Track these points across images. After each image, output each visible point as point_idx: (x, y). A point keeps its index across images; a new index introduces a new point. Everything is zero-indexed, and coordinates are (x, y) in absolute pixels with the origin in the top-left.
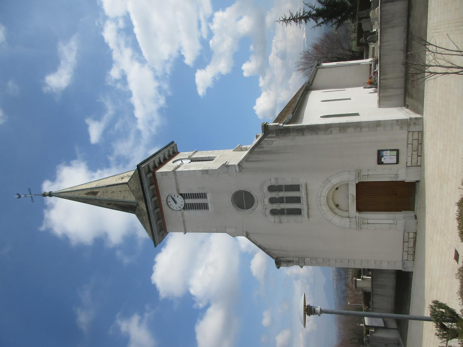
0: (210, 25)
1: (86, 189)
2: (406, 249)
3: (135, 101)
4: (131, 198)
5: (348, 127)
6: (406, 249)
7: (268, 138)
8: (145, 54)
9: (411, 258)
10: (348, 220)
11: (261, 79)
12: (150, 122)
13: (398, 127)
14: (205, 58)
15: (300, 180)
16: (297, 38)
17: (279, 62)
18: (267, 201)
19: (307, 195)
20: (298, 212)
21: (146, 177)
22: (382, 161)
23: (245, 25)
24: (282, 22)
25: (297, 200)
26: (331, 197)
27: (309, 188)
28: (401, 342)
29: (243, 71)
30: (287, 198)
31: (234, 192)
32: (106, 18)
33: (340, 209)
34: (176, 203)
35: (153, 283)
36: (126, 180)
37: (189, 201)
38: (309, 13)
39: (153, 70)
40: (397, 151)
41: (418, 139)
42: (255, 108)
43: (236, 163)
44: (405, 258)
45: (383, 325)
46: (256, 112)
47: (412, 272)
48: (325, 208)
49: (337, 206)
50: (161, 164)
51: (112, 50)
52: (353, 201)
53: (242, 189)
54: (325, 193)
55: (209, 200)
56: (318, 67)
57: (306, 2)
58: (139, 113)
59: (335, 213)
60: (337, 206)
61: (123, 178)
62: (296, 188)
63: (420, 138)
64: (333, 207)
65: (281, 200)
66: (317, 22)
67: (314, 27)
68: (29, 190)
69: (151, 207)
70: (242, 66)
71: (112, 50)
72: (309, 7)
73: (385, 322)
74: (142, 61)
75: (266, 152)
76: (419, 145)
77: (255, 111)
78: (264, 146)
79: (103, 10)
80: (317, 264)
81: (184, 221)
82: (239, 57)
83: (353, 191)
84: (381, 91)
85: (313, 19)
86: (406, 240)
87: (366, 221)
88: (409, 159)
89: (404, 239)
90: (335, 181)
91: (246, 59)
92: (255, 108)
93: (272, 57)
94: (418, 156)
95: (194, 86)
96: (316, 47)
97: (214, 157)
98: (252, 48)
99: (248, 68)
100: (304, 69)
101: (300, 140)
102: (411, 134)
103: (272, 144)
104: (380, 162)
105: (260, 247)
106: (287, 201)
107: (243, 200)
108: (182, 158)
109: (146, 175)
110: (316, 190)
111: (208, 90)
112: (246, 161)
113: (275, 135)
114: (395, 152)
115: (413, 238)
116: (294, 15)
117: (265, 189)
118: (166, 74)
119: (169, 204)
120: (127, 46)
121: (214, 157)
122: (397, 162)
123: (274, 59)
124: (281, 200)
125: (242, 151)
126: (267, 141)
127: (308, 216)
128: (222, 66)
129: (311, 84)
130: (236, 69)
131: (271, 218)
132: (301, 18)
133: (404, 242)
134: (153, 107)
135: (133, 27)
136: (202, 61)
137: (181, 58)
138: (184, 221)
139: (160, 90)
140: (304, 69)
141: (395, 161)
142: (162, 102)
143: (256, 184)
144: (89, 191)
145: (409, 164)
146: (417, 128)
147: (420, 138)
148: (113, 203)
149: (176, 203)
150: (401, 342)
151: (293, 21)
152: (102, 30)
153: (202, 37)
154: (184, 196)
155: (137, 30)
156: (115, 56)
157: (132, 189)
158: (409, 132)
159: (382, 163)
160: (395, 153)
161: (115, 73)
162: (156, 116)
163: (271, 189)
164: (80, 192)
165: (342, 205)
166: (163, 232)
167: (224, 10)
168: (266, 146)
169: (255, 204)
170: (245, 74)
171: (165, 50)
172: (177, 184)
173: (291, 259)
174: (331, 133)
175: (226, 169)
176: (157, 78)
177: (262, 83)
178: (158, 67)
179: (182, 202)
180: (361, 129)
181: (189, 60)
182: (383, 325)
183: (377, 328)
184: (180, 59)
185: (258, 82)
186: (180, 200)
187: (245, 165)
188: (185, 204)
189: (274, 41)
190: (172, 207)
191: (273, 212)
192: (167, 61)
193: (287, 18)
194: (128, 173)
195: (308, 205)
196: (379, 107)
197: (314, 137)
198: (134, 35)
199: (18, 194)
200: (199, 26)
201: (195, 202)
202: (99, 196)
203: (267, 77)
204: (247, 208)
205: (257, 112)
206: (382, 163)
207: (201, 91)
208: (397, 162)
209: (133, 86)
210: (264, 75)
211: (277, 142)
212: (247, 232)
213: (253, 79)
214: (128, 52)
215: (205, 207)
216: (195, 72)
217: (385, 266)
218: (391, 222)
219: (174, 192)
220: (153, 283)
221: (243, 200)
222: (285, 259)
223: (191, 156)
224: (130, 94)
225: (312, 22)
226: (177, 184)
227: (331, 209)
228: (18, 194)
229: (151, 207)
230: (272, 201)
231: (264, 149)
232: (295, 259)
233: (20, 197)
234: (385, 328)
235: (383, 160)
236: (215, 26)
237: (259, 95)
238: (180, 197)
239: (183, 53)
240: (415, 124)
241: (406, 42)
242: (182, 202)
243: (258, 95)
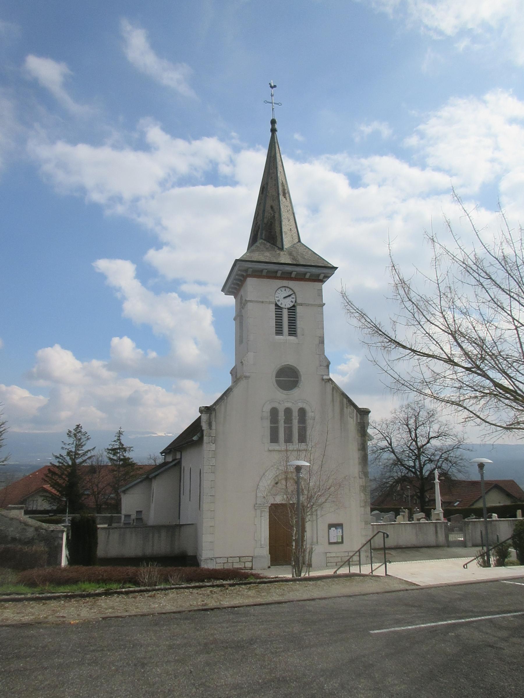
0: (198, 299)
2: (230, 560)
3: (105, 153)
6: (230, 560)
7: (357, 414)
8: (177, 191)
20: (274, 439)
22: (332, 529)
23: (188, 351)
29: (121, 337)
31: (279, 367)
32: (237, 150)
37: (285, 313)
40: (342, 542)
42: (57, 347)
43: (331, 376)
44: (219, 561)
46: (50, 349)
58: (83, 152)
62: (302, 439)
70: (129, 337)
71: (190, 143)
74: (163, 184)
75: (342, 410)
77: (52, 346)
78: (349, 409)
79: (248, 148)
81: (263, 302)
82: (145, 334)
86: (243, 560)
88: (333, 555)
89: (243, 557)
91: (139, 344)
92: (57, 347)
94: (336, 563)
98: (153, 354)
103: (350, 417)
104: (330, 526)
111: (103, 277)
112: (333, 388)
114: (340, 541)
115: (245, 567)
117: (300, 405)
118: (139, 215)
122: (330, 543)
126: (354, 412)
128: (136, 303)
131: (267, 408)
133: (240, 557)
135: (216, 185)
136: (146, 274)
137: (158, 245)
138: (263, 302)
139: (118, 199)
142: (96, 197)
143: (307, 395)
145: (328, 555)
148: (277, 215)
152: (222, 140)
153: (185, 282)
155: (210, 189)
156: (181, 144)
161: (155, 134)
163: (302, 412)
167: (213, 323)
169: (285, 392)
170: (116, 340)
172: (308, 305)
173: (214, 427)
174: (360, 478)
175: (325, 364)
176: (136, 199)
177: (96, 363)
179: (285, 305)
180: (363, 507)
181: (155, 257)
186: (287, 303)
187: (329, 386)
189: (159, 388)
191: (274, 412)
192: (158, 223)
197: (357, 461)
198: (204, 184)
200: (200, 283)
203: (105, 373)
204: (277, 381)
205: (49, 351)
207: (103, 264)
208: (330, 543)
209: (130, 158)
210: (110, 367)
211: (352, 423)
212: (249, 377)
213: (103, 351)
214: (183, 167)
216: (133, 262)
222: (214, 420)
226: (308, 305)
228: (275, 86)
231: (345, 409)
236: (193, 306)
242: (285, 305)
243: (79, 355)
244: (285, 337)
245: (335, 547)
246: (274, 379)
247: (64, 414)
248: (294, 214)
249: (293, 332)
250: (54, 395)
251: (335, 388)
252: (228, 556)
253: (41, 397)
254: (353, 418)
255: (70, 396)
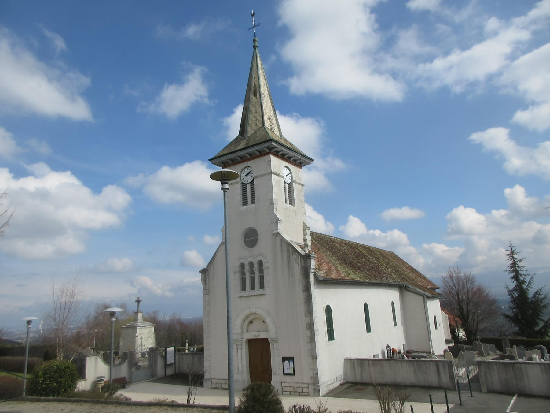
1: (259, 85)
2: (220, 381)
3: (455, 57)
4: (250, 131)
5: (311, 331)
6: (220, 381)
9: (214, 386)
10: (239, 331)
11: (503, 212)
12: (429, 79)
13: (312, 375)
14: (526, 138)
15: (268, 290)
16: (489, 269)
17: (530, 235)
18: (251, 259)
19: (257, 295)
21: (265, 147)
24: (510, 249)
25: (253, 287)
26: (257, 316)
27: (262, 297)
28: (155, 378)
30: (254, 277)
31: (257, 229)
33: (248, 325)
34: (247, 175)
35: (234, 110)
36: (267, 124)
37: (249, 187)
38: (524, 282)
39: (500, 74)
40: (294, 374)
41: (303, 392)
43: (279, 231)
44: (214, 381)
45: (167, 363)
47: (203, 387)
48: (247, 312)
49: (251, 322)
50: (283, 157)
51: (524, 14)
52: (255, 336)
53: (259, 237)
54: (259, 311)
55: (250, 206)
56: (425, 297)
57: (535, 277)
59: (244, 321)
60: (251, 322)
61: (270, 119)
62: (262, 286)
63: (304, 394)
64: (250, 319)
65: (252, 272)
66: (513, 290)
67: (507, 287)
68: (259, 25)
69: (240, 153)
70: (521, 185)
72: (530, 281)
73: (171, 365)
74: (512, 57)
75: (289, 257)
76: (298, 394)
80: (205, 306)
83: (262, 336)
84: (359, 361)
85: (516, 286)
87: (239, 347)
88: (287, 385)
90: (268, 320)
91: (529, 193)
92: (461, 208)
93: (536, 226)
95: (483, 127)
96: (480, 290)
97: (294, 205)
99: (518, 194)
100: (451, 277)
101: (299, 288)
102: (306, 386)
104: (284, 359)
105: (215, 255)
106: (252, 277)
107: (251, 238)
108: (293, 174)
109: (258, 151)
110: (262, 304)
111: (480, 146)
113: (303, 265)
116: (520, 264)
119: (246, 169)
120: (535, 33)
121: (294, 205)
123: (533, 228)
124: (252, 272)
125: (304, 230)
127: (241, 297)
128: (516, 162)
129: (406, 290)
130: (512, 180)
131: (237, 264)
132: (517, 272)
134: (449, 79)
139: (473, 84)
140: (451, 277)
141: (286, 372)
142: (458, 89)
143: (264, 249)
144: (258, 88)
146: (311, 392)
147: (304, 394)
149: (247, 175)
150: (155, 378)
151: (511, 262)
154: (252, 182)
156: (519, 20)
157: (258, 132)
158: (308, 384)
159: (283, 361)
160: (292, 372)
161: (492, 23)
162: (437, 85)
163: (261, 263)
164: (256, 78)
165: (252, 326)
166: (223, 165)
168: (294, 257)
169: (248, 249)
171: (533, 85)
172: (261, 176)
173: (207, 282)
176: (490, 77)
177: (499, 214)
178: (505, 79)
180: (310, 343)
181: (521, 117)
182: (167, 363)
183: (165, 358)
184: (523, 103)
185: (497, 209)
188: (246, 184)
190: (243, 172)
191: (242, 266)
192: (515, 88)
193: (515, 256)
194: (275, 123)
195: (249, 296)
196: (345, 359)
199: (254, 13)
201: (248, 195)
202: (253, 98)
204: (245, 242)
206: (283, 361)
207: (476, 137)
209: (478, 50)
211: (297, 268)
215: (245, 203)
217: (206, 364)
218: (240, 369)
219: (255, 174)
220: (234, 110)
221: (251, 238)
223: (296, 182)
224: (465, 47)
225: (512, 285)
226: (261, 176)
227: (248, 317)
229: (240, 153)
230: (251, 264)
231: (291, 256)
232: (207, 286)
233: (253, 16)
234: (166, 366)
235: (286, 362)
237: (479, 211)
238: (252, 179)
239: (531, 108)
240: (315, 389)
241: (402, 384)
244: (289, 205)
245: (288, 378)
246: (243, 240)
247: (480, 258)
248: (262, 106)
249: (253, 202)
250: (468, 244)
251: (283, 240)
252: (219, 378)
253: (457, 248)
254: (297, 263)
255: (482, 244)
